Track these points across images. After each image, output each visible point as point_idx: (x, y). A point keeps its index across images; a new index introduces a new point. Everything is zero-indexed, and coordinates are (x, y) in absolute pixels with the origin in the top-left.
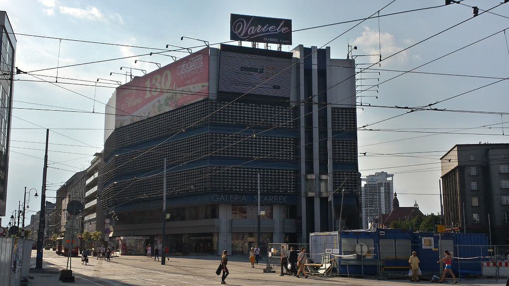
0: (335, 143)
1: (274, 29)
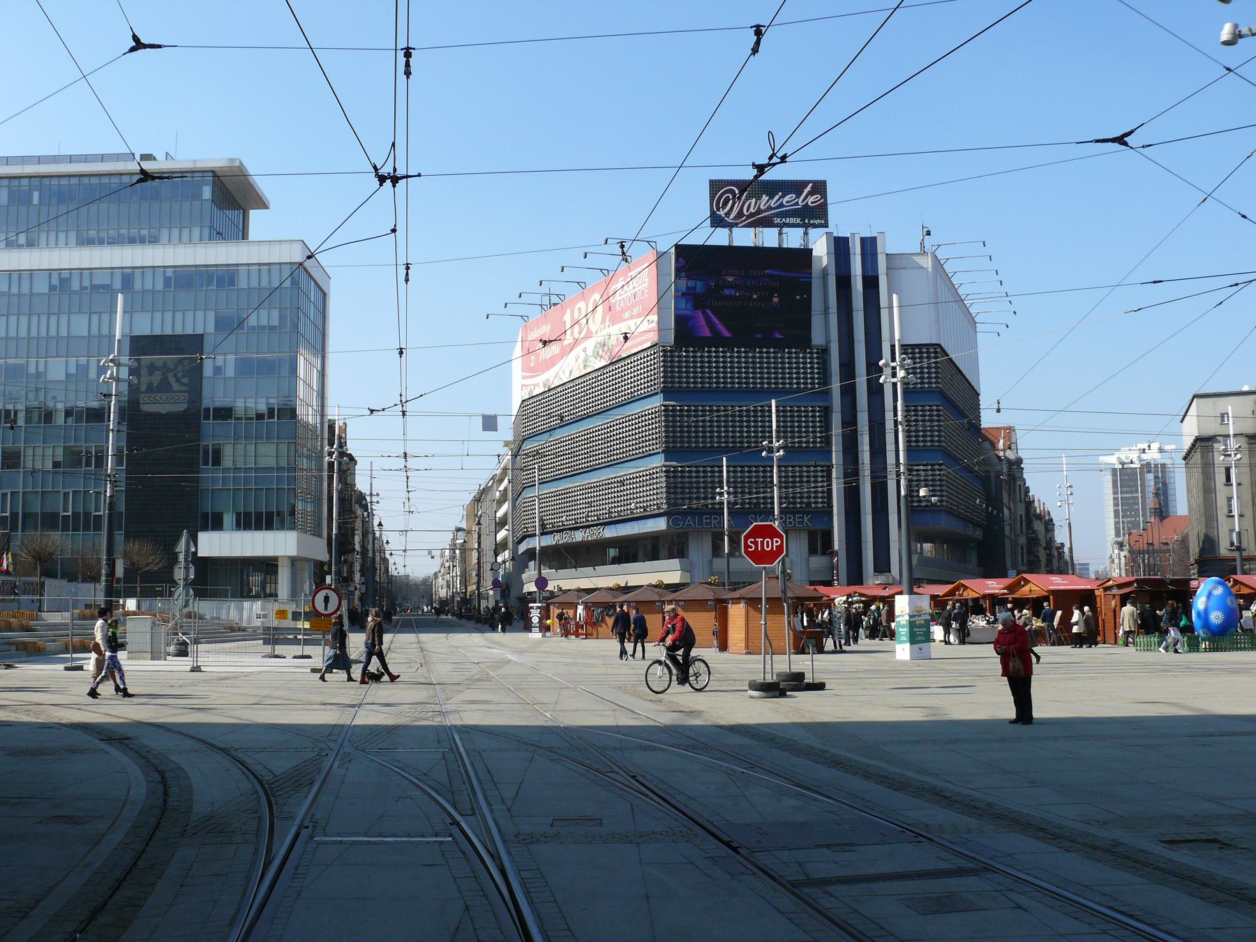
1: (795, 199)
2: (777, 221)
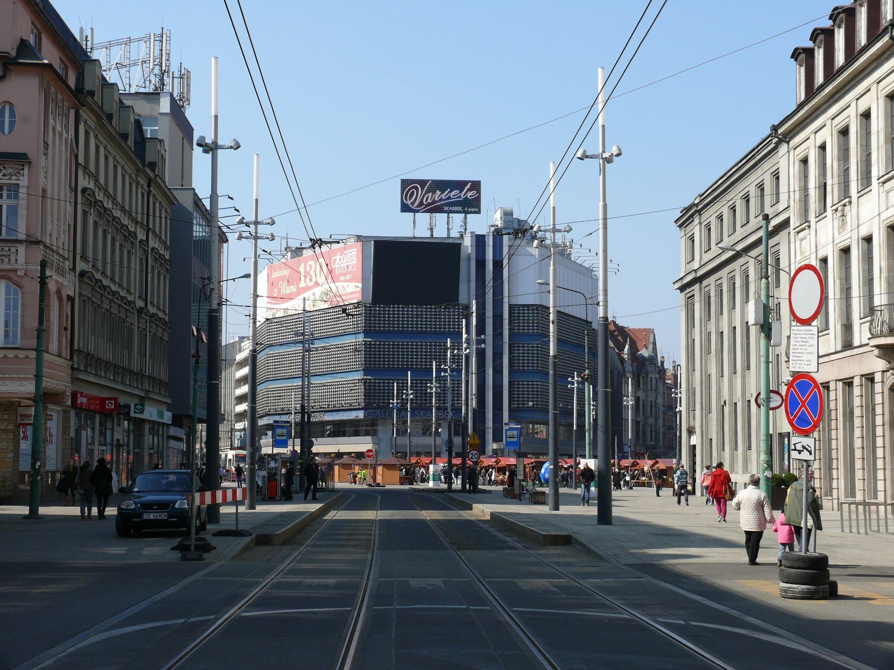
2: (446, 208)
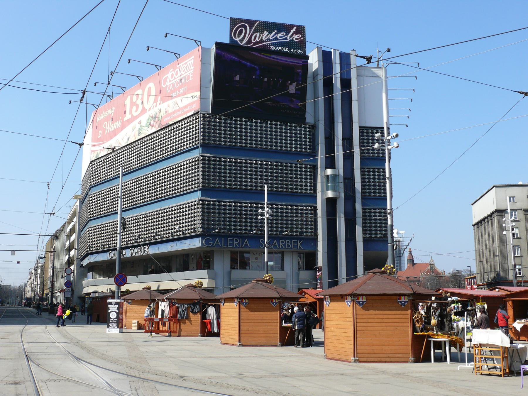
0: (365, 171)
1: (285, 36)
